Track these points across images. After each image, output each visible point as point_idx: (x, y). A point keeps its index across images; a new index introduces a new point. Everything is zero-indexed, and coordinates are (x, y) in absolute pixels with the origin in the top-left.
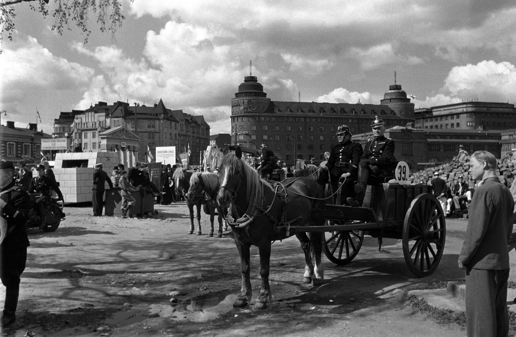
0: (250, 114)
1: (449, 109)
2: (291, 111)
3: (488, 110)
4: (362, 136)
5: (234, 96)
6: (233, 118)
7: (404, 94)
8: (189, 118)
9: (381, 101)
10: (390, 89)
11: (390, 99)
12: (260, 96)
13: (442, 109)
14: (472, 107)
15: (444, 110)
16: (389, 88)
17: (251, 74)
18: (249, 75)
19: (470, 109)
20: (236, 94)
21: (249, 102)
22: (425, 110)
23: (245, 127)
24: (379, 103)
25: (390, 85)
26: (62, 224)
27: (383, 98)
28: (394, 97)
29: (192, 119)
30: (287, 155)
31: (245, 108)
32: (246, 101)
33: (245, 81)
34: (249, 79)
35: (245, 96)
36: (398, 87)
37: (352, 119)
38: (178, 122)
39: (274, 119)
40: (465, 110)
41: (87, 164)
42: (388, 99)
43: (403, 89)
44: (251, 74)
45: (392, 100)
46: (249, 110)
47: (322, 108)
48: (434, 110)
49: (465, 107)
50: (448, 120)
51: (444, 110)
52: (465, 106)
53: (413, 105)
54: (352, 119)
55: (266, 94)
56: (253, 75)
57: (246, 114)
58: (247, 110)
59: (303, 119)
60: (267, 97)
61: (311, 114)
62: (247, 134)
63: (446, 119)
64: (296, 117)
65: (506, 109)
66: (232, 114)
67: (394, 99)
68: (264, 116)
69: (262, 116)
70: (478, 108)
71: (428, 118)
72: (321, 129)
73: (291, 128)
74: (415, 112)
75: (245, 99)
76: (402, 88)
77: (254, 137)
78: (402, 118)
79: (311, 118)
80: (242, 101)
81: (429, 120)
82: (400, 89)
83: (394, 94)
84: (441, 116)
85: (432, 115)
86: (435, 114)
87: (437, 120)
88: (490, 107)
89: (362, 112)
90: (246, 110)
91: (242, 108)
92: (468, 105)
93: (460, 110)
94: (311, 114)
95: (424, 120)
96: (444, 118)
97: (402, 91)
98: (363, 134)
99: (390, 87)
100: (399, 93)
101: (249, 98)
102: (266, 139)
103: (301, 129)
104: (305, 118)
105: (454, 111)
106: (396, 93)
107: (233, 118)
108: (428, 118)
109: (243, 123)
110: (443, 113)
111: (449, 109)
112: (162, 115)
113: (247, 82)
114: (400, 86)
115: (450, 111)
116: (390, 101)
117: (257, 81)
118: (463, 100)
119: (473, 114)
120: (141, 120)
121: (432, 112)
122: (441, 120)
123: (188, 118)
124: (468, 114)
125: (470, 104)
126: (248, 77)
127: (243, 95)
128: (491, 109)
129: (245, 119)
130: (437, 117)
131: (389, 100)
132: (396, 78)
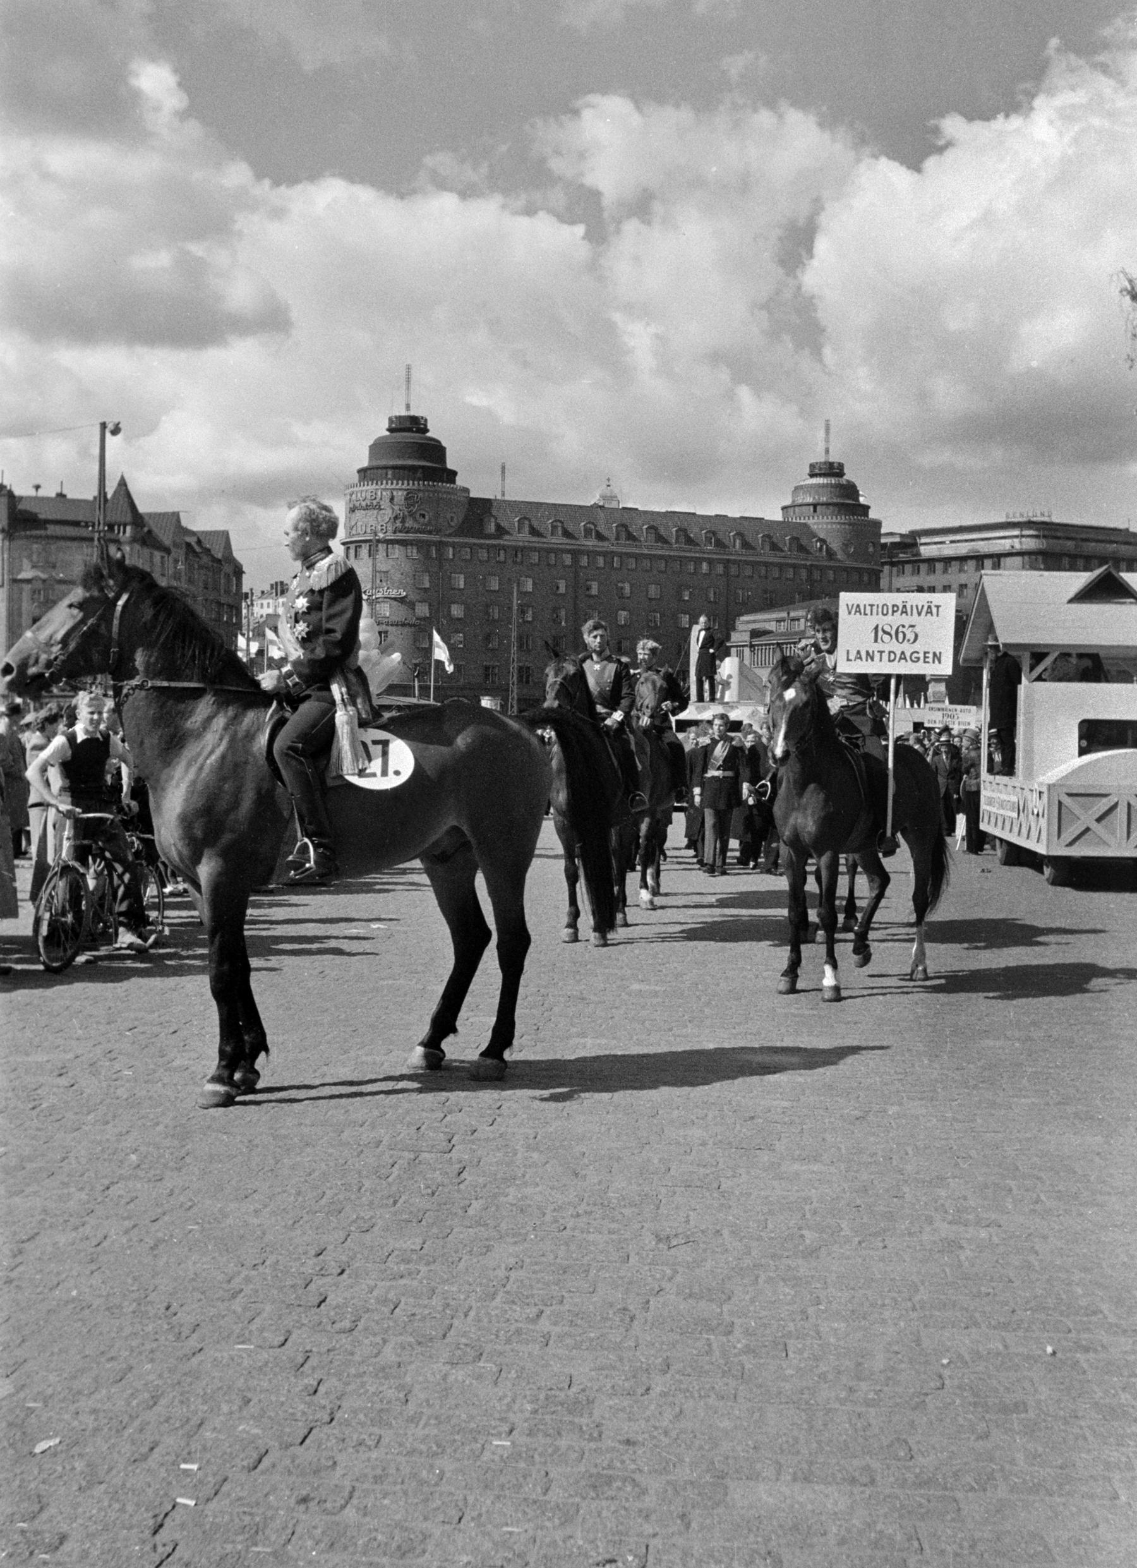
0: (411, 536)
1: (966, 541)
2: (534, 532)
3: (1076, 546)
4: (779, 621)
5: (356, 478)
6: (352, 546)
7: (851, 490)
8: (192, 540)
9: (784, 508)
10: (812, 475)
11: (815, 506)
12: (443, 482)
13: (948, 538)
14: (1037, 537)
15: (952, 542)
16: (808, 470)
17: (408, 407)
18: (403, 413)
19: (1030, 544)
20: (363, 472)
21: (409, 497)
22: (897, 539)
23: (397, 576)
24: (778, 516)
25: (813, 461)
26: (260, 1085)
27: (788, 502)
28: (824, 499)
29: (199, 542)
30: (487, 668)
31: (396, 518)
32: (400, 496)
33: (388, 430)
34: (408, 424)
35: (839, 513)
36: (833, 470)
37: (710, 562)
38: (168, 551)
39: (483, 555)
40: (1017, 546)
41: (933, 941)
42: (808, 505)
43: (849, 475)
44: (408, 407)
45: (818, 508)
46: (409, 523)
47: (624, 526)
48: (924, 540)
49: (1016, 537)
50: (965, 572)
51: (952, 542)
52: (1016, 532)
53: (877, 524)
54: (710, 562)
55: (866, 508)
56: (413, 412)
57: (400, 536)
58: (403, 522)
59: (568, 559)
60: (460, 481)
61: (591, 543)
62: (401, 600)
63: (961, 570)
64: (549, 551)
65: (1123, 548)
66: (350, 535)
67: (827, 504)
68: (453, 545)
69: (447, 544)
70: (1051, 541)
71: (908, 562)
72: (622, 588)
73: (534, 584)
74: (883, 541)
75: (399, 489)
76: (846, 471)
77: (423, 610)
78: (849, 563)
79: (592, 554)
80: (386, 494)
81: (908, 567)
82: (841, 474)
83: (825, 490)
84: (947, 561)
85: (918, 554)
86: (926, 551)
87: (932, 570)
88: (1083, 540)
89: (738, 542)
90: (398, 524)
91: (388, 513)
92: (1026, 532)
93: (1005, 545)
94: (591, 543)
95: (895, 569)
96: (955, 565)
97: (848, 481)
98: (784, 615)
99: (812, 466)
100: (840, 486)
101: (412, 485)
102: (461, 615)
103: (562, 590)
104: (576, 554)
105: (984, 547)
106: (831, 485)
107: (352, 546)
108: (908, 562)
109: (391, 562)
110: (949, 550)
111: (966, 541)
112: (128, 529)
113: (395, 434)
114: (841, 466)
115: (969, 546)
116: (815, 511)
117: (427, 431)
118: (1007, 517)
119: (1040, 558)
120: (62, 543)
121: (915, 545)
122: (945, 571)
123: (188, 539)
124: (1026, 558)
125: (1031, 528)
126: (400, 418)
127: (419, 475)
128: (1084, 544)
129: (397, 551)
130: (931, 561)
131: (812, 508)
132: (408, 395)
